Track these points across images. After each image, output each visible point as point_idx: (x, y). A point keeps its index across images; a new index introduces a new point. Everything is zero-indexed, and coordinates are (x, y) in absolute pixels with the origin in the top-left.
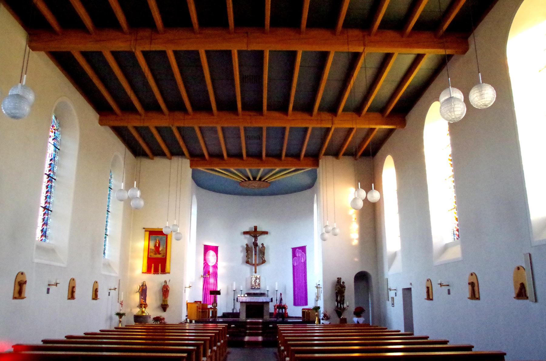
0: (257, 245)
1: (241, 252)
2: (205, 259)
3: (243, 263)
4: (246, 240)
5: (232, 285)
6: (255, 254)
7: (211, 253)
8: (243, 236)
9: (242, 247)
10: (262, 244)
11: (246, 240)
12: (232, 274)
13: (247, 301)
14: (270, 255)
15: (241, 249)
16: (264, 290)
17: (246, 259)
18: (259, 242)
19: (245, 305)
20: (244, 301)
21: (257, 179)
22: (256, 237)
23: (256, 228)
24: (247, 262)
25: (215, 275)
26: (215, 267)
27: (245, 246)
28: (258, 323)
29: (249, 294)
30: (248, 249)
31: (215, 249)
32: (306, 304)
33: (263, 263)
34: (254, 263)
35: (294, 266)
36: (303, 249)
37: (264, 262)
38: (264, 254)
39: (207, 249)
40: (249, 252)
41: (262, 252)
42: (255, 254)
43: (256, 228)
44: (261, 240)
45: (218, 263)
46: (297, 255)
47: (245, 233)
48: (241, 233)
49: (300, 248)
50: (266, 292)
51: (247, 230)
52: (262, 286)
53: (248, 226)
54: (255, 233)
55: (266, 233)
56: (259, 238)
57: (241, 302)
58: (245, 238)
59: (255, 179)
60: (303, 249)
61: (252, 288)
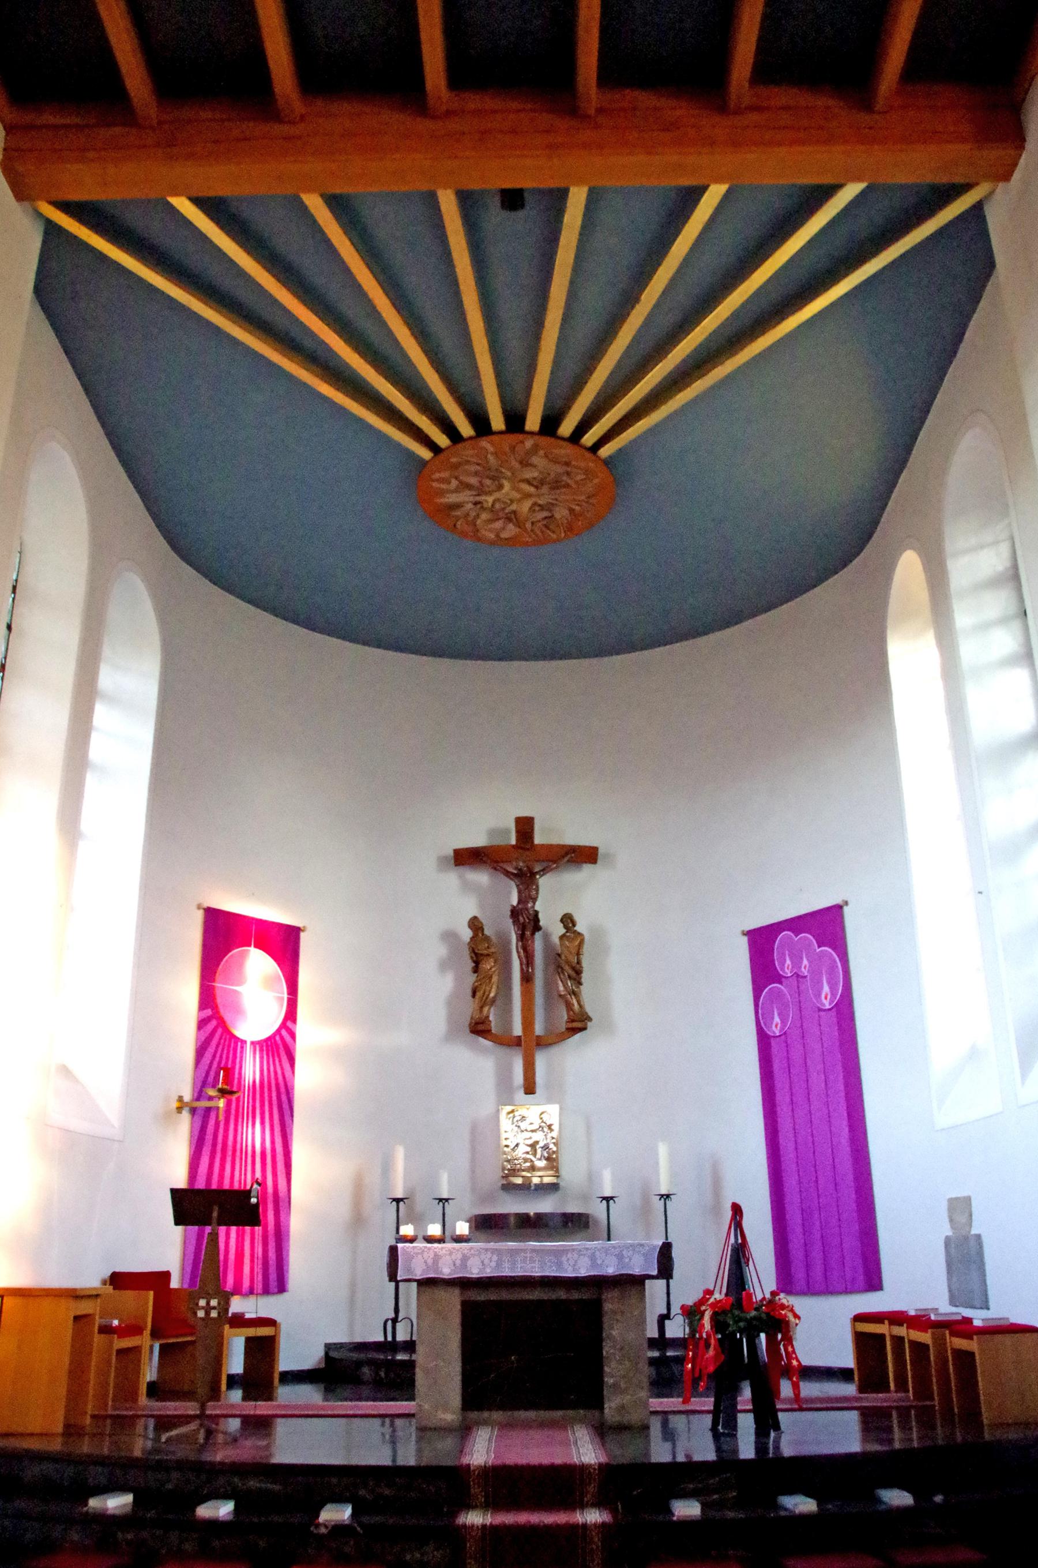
0: (535, 925)
1: (444, 966)
2: (208, 998)
3: (451, 1035)
4: (467, 900)
5: (387, 1168)
6: (523, 985)
7: (257, 965)
8: (452, 878)
9: (449, 936)
10: (568, 921)
11: (467, 900)
12: (384, 1099)
13: (475, 1271)
14: (615, 982)
15: (442, 950)
16: (585, 1198)
17: (468, 1008)
18: (549, 908)
19: (453, 1301)
20: (446, 1272)
21: (533, 422)
22: (526, 880)
23: (525, 826)
24: (479, 1028)
25: (278, 1101)
26: (280, 1047)
27: (467, 934)
28: (561, 1484)
29: (487, 1224)
30: (480, 951)
31: (283, 944)
32: (873, 1282)
33: (573, 1031)
34: (518, 1030)
35: (764, 1040)
36: (826, 926)
37: (578, 1023)
38: (577, 973)
39: (224, 934)
40: (487, 965)
41: (569, 965)
42: (527, 979)
43: (525, 826)
44: (555, 896)
45: (303, 1027)
46: (787, 968)
47: (467, 858)
48: (442, 861)
49: (796, 924)
50: (598, 1210)
51: (478, 840)
52: (572, 1173)
53: (484, 822)
54: (522, 858)
55: (587, 855)
56: (545, 882)
57: (426, 1284)
58: (467, 887)
59: (515, 421)
60: (826, 926)
61: (508, 1188)
